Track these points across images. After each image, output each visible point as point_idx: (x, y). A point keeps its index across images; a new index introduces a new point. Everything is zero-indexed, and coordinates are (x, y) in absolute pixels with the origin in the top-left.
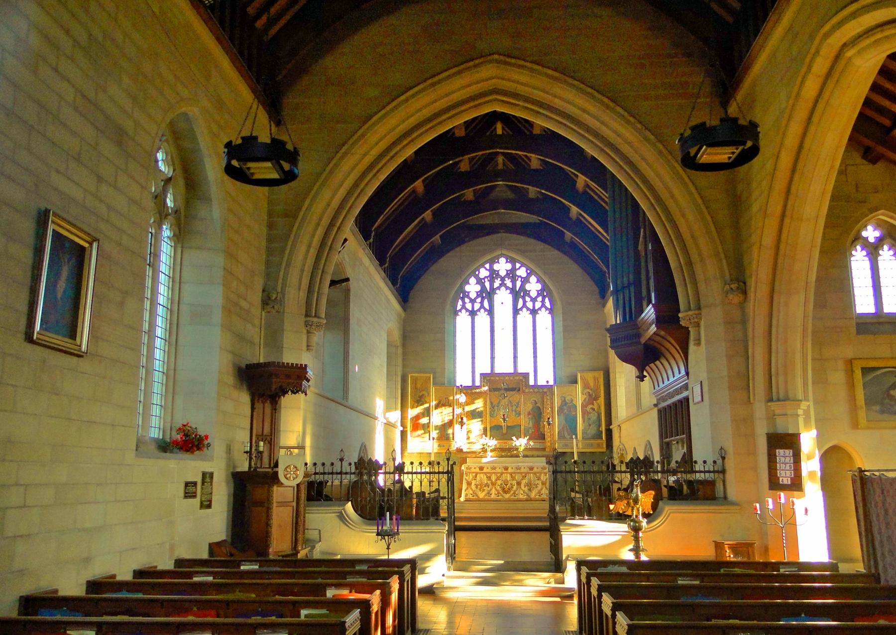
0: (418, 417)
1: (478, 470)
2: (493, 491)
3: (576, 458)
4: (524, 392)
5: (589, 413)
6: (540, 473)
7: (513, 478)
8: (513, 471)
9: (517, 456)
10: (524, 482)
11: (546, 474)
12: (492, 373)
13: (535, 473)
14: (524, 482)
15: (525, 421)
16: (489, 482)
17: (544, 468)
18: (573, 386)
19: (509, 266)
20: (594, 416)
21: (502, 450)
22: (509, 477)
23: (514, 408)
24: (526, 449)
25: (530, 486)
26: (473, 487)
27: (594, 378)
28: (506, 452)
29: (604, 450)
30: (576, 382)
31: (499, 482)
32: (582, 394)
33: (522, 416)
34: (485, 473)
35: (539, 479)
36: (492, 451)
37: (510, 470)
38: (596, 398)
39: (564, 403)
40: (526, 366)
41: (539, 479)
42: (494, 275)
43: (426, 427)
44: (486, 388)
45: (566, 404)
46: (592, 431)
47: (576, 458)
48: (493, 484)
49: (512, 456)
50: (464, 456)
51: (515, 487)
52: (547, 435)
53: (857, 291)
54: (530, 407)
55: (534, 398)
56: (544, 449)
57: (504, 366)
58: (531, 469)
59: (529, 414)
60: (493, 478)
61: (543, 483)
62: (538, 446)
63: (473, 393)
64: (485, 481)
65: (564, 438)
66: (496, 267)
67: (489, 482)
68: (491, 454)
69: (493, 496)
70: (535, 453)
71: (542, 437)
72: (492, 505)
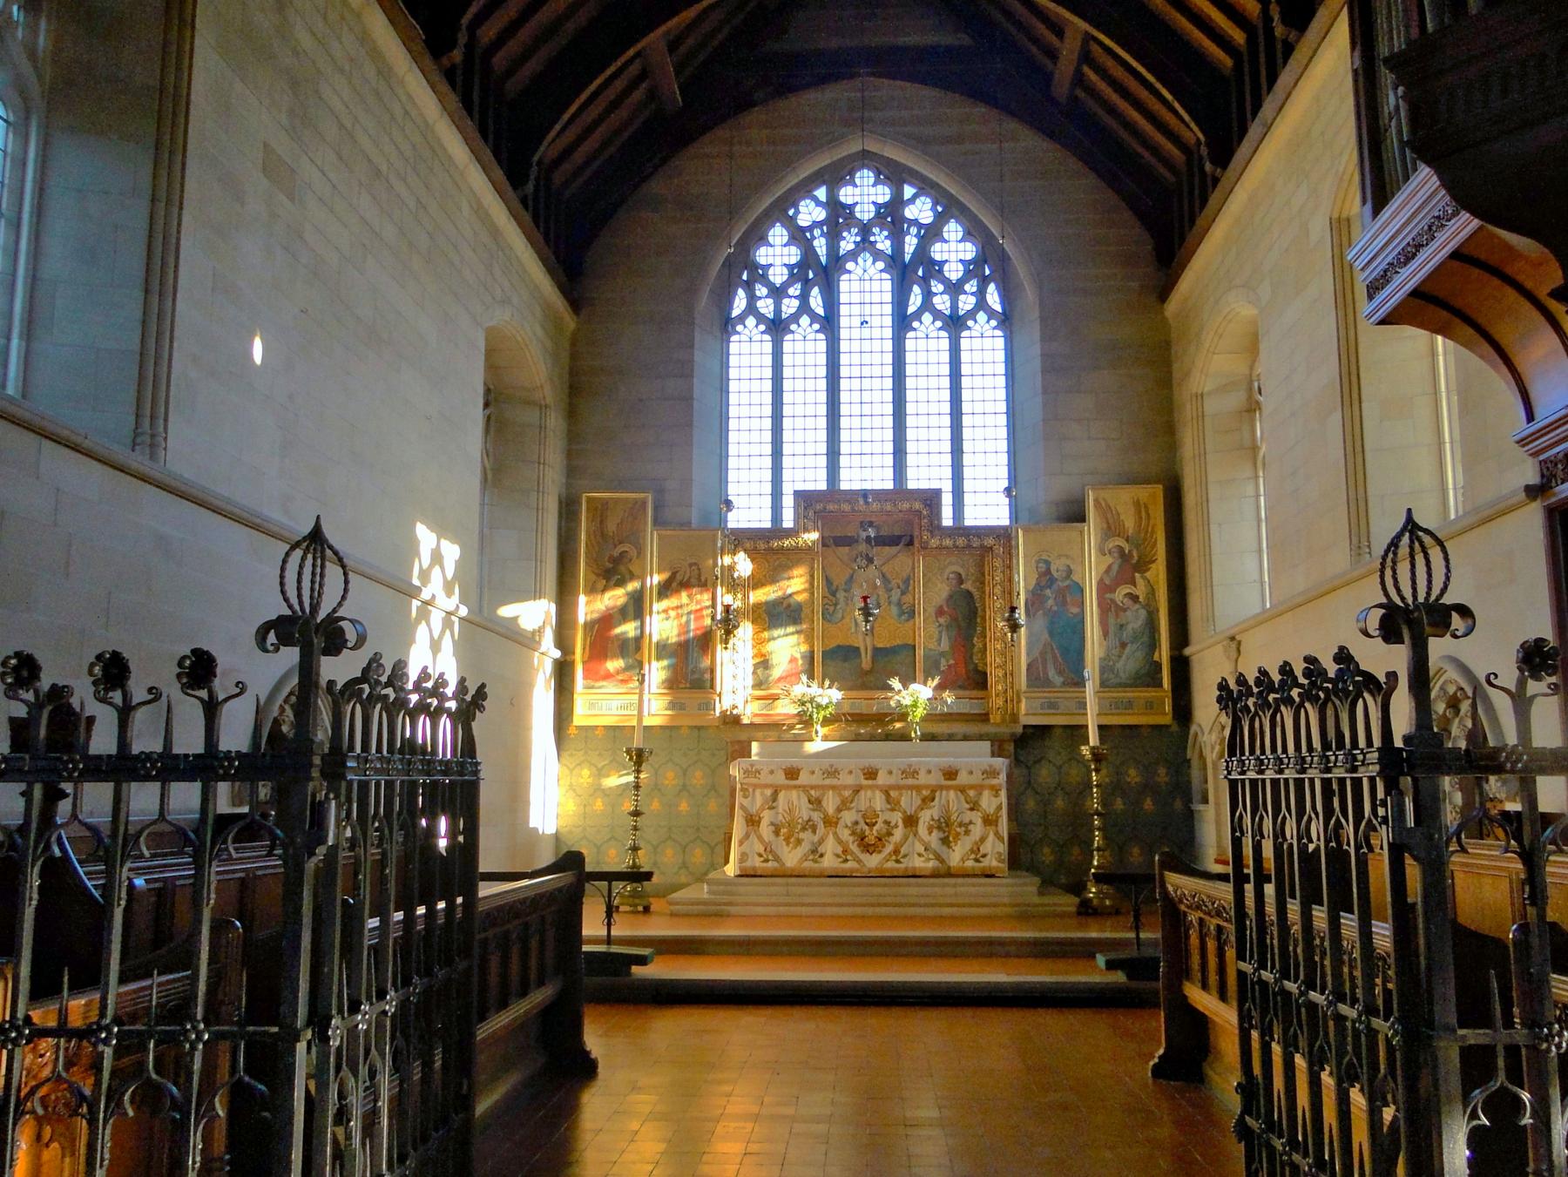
0: (605, 622)
1: (780, 778)
2: (830, 847)
4: (924, 547)
6: (979, 788)
7: (893, 804)
8: (892, 780)
9: (904, 737)
11: (995, 790)
13: (962, 790)
14: (926, 817)
15: (928, 635)
16: (816, 816)
17: (991, 773)
19: (883, 194)
20: (1135, 619)
21: (859, 718)
22: (879, 802)
24: (929, 718)
25: (947, 829)
26: (765, 830)
27: (1137, 504)
30: (1081, 518)
31: (848, 817)
33: (920, 620)
34: (804, 789)
36: (826, 722)
37: (882, 779)
38: (1142, 565)
39: (1045, 578)
40: (927, 472)
42: (839, 215)
43: (632, 649)
45: (1052, 580)
46: (1130, 662)
47: (1093, 738)
48: (830, 822)
49: (888, 737)
50: (744, 737)
51: (898, 834)
52: (994, 675)
54: (942, 591)
55: (954, 566)
56: (984, 718)
57: (867, 472)
58: (951, 774)
59: (940, 612)
61: (989, 821)
62: (966, 707)
64: (804, 811)
65: (1047, 683)
66: (847, 195)
67: (816, 816)
68: (823, 731)
69: (829, 862)
70: (959, 728)
71: (979, 681)
72: (821, 892)
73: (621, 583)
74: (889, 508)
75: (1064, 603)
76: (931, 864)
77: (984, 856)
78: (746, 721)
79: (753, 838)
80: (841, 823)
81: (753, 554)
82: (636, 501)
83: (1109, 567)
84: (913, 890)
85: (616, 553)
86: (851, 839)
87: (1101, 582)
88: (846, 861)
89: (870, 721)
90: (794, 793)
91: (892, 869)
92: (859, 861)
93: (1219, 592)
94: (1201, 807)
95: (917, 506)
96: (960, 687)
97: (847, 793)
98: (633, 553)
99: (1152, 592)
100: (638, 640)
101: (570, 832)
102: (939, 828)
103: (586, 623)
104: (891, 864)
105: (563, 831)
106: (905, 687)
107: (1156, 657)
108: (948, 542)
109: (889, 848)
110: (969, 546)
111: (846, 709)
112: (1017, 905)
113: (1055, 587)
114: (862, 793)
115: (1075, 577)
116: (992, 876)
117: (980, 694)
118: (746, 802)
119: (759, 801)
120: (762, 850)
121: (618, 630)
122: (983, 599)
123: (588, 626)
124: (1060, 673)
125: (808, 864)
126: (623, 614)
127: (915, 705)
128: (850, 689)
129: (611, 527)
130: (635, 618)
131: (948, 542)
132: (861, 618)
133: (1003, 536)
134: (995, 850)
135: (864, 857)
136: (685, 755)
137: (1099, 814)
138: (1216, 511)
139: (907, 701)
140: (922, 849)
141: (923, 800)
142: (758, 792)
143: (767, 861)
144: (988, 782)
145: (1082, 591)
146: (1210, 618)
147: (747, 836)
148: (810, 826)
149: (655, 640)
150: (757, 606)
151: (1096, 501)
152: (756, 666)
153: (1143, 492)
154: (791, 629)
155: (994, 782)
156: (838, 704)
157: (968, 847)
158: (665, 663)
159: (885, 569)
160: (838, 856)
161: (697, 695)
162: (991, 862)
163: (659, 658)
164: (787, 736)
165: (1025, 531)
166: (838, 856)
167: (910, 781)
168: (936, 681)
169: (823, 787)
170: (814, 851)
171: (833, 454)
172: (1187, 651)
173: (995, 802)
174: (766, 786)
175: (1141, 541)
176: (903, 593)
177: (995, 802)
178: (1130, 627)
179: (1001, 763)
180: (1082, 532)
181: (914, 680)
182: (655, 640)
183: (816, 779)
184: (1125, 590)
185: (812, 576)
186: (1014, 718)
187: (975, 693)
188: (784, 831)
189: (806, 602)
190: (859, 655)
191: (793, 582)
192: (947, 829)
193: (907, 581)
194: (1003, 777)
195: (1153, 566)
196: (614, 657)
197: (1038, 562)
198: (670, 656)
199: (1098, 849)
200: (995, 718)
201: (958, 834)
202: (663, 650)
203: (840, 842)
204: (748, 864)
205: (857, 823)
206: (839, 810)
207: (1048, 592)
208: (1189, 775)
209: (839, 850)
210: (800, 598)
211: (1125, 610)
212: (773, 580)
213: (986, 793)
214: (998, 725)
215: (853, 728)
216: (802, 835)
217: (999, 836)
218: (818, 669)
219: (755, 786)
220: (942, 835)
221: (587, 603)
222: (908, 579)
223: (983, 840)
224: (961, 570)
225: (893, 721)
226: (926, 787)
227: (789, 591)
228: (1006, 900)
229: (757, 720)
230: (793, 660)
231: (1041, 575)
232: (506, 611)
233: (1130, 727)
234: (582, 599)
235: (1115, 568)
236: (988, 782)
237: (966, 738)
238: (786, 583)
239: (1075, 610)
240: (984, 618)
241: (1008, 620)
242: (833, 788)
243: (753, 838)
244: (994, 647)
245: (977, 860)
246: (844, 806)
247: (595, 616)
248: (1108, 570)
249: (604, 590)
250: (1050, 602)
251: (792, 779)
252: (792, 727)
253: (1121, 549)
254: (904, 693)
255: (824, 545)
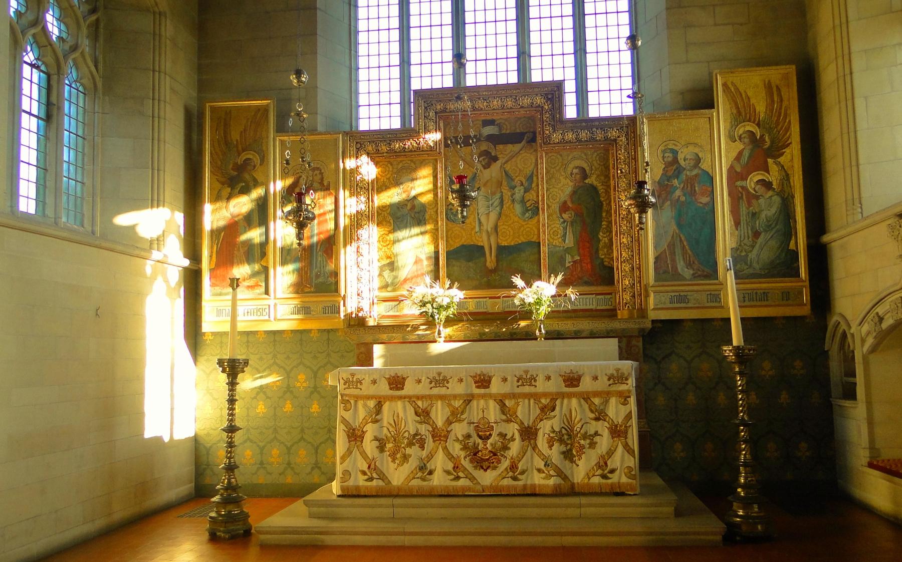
0: (232, 229)
1: (384, 388)
2: (440, 462)
3: (737, 338)
4: (547, 141)
5: (753, 197)
6: (606, 395)
7: (508, 414)
8: (506, 389)
9: (528, 336)
10: (546, 428)
11: (624, 398)
12: (459, 91)
13: (586, 397)
14: (546, 428)
15: (553, 232)
16: (424, 429)
17: (618, 378)
18: (699, 120)
20: (769, 207)
21: (479, 317)
22: (493, 413)
23: (519, 192)
24: (552, 315)
25: (569, 441)
26: (369, 446)
27: (769, 87)
28: (498, 325)
29: (806, 311)
30: (709, 104)
31: (459, 429)
32: (732, 138)
33: (543, 217)
34: (411, 399)
35: (600, 416)
36: (449, 322)
37: (496, 387)
38: (776, 150)
39: (673, 167)
40: (551, 65)
41: (600, 416)
43: (257, 253)
44: (433, 137)
45: (679, 171)
46: (764, 252)
47: (737, 338)
48: (440, 436)
49: (514, 336)
50: (369, 339)
51: (515, 447)
52: (621, 269)
53: (798, 133)
54: (565, 188)
55: (577, 161)
56: (611, 314)
57: (490, 67)
58: (572, 380)
59: (564, 208)
60: (439, 415)
61: (617, 432)
62: (592, 303)
63: (392, 151)
64: (411, 424)
65: (677, 276)
67: (424, 429)
68: (446, 332)
69: (439, 480)
70: (585, 325)
71: (605, 276)
72: (433, 509)
73: (245, 191)
74: (509, 103)
75: (693, 193)
76: (551, 482)
77: (612, 471)
78: (371, 323)
79: (356, 453)
80: (452, 436)
81: (375, 158)
82: (258, 109)
83: (740, 154)
84: (531, 508)
85: (240, 161)
86: (462, 454)
87: (731, 170)
88: (458, 478)
89: (494, 320)
90: (400, 404)
91: (508, 487)
92: (472, 479)
93: (866, 173)
94: (847, 403)
95: (539, 100)
96: (587, 283)
97: (457, 403)
98: (257, 159)
99: (786, 177)
100: (264, 245)
101: (208, 435)
102: (561, 441)
103: (212, 231)
104: (507, 482)
105: (202, 433)
106: (529, 284)
107: (792, 246)
108: (570, 136)
109: (506, 464)
110: (592, 140)
111: (472, 307)
112: (651, 534)
113: (683, 177)
114: (474, 403)
115: (705, 165)
116: (622, 494)
117: (606, 289)
118: (348, 415)
119: (362, 413)
120: (365, 467)
121: (244, 237)
122: (607, 192)
123: (214, 233)
124: (689, 265)
125: (416, 483)
126: (249, 221)
127: (539, 303)
128: (475, 288)
129: (235, 136)
130: (260, 225)
131: (570, 136)
132: (456, 203)
133: (628, 125)
134: (624, 462)
135: (478, 474)
136: (315, 357)
137: (745, 425)
138: (862, 82)
139: (530, 300)
140: (541, 465)
141: (542, 409)
142: (360, 403)
143: (371, 479)
144: (615, 388)
145: (711, 179)
146: (856, 200)
147: (349, 452)
148: (417, 440)
149: (279, 245)
150: (382, 209)
151: (725, 85)
152: (382, 269)
153: (774, 74)
154: (416, 230)
155: (623, 387)
156: (460, 304)
157: (594, 462)
158: (291, 267)
159: (508, 167)
160: (448, 472)
161: (325, 299)
162: (620, 478)
163: (284, 263)
164: (412, 337)
165: (651, 119)
166: (448, 472)
167: (527, 389)
168: (560, 278)
169: (430, 397)
170: (422, 468)
171: (459, 58)
172: (826, 238)
173: (623, 411)
174: (369, 398)
175: (773, 126)
176: (526, 191)
177: (622, 411)
178: (763, 216)
179: (628, 366)
180: (710, 119)
181: (539, 278)
182: (279, 245)
183: (423, 389)
184: (756, 177)
185: (435, 177)
186: (643, 312)
187: (600, 289)
188: (389, 446)
189: (430, 203)
190: (484, 254)
191: (417, 183)
192: (569, 441)
193: (530, 178)
194: (632, 382)
195: (787, 150)
196: (241, 262)
197: (664, 152)
198: (295, 260)
199: (745, 465)
200: (622, 314)
201: (582, 447)
202: (287, 255)
203: (450, 456)
204: (351, 483)
205: (468, 436)
206: (449, 422)
207: (675, 182)
208: (827, 367)
209: (450, 466)
210: (425, 199)
211: (757, 198)
212: (397, 183)
213: (613, 401)
214: (626, 321)
215: (477, 328)
216: (408, 451)
217: (628, 449)
218: (443, 272)
219: (357, 398)
220: (563, 448)
221: (214, 211)
222: (531, 176)
223: (611, 453)
224: (585, 166)
225: (515, 320)
226: (545, 395)
227: (413, 193)
228: (638, 529)
229: (386, 322)
230: (418, 261)
231: (668, 165)
232: (123, 220)
233: (795, 318)
234: (208, 208)
235: (746, 154)
236: (615, 388)
237: (593, 335)
238: (410, 185)
239: (705, 200)
240: (609, 212)
241: (633, 198)
242: (442, 397)
243: (356, 453)
244: (620, 226)
245: (604, 477)
246: (455, 416)
247: (222, 223)
248: (738, 158)
249: (229, 199)
250: (678, 193)
251: (398, 389)
252: (416, 328)
253: (752, 134)
254: (527, 291)
255: (447, 145)
